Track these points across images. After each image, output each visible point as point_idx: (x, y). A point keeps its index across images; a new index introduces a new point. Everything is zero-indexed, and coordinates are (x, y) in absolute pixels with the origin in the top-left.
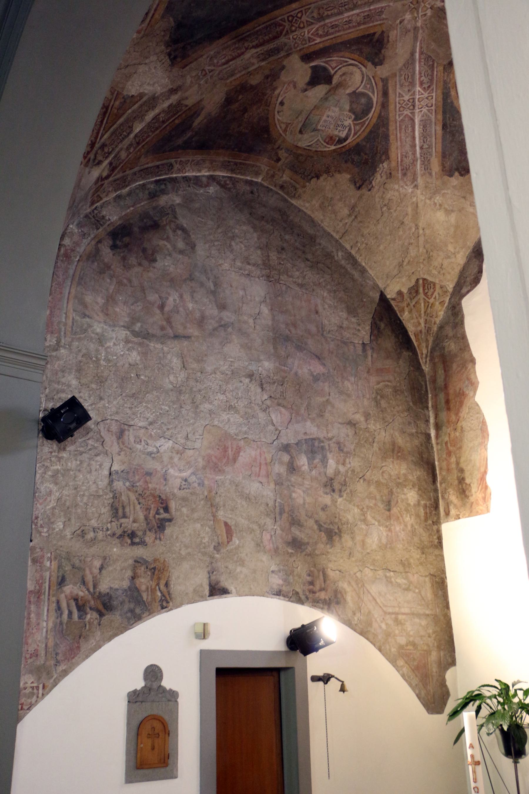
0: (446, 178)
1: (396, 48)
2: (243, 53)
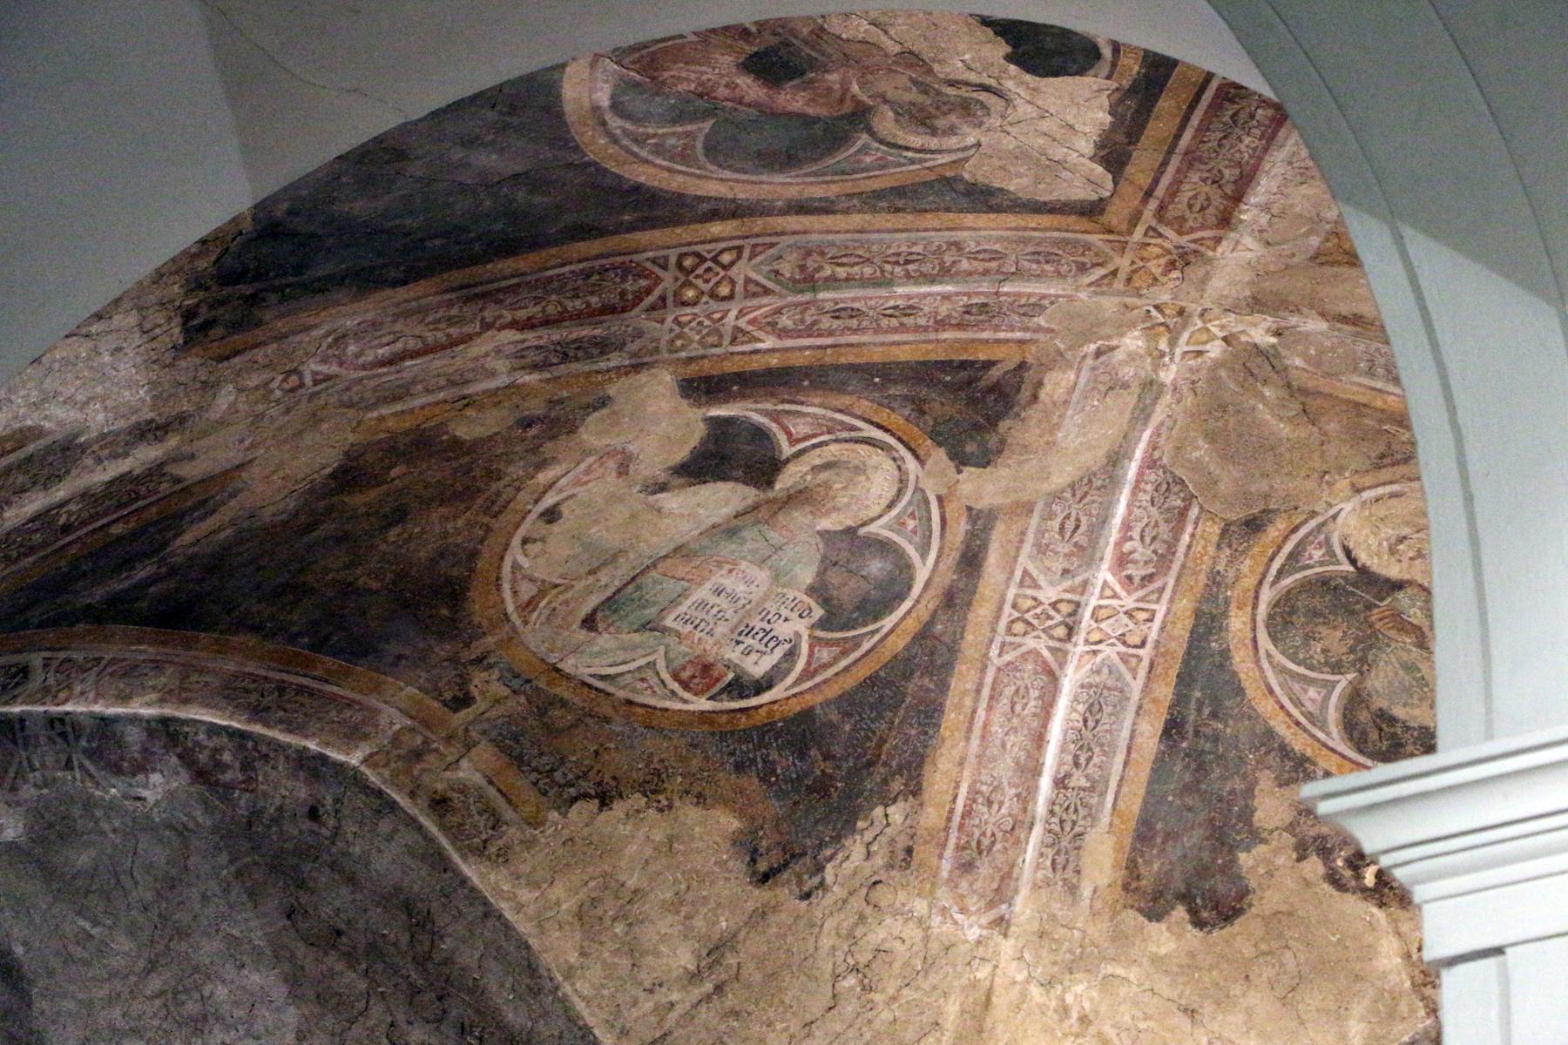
0: (1132, 918)
1: (1058, 426)
2: (467, 339)
